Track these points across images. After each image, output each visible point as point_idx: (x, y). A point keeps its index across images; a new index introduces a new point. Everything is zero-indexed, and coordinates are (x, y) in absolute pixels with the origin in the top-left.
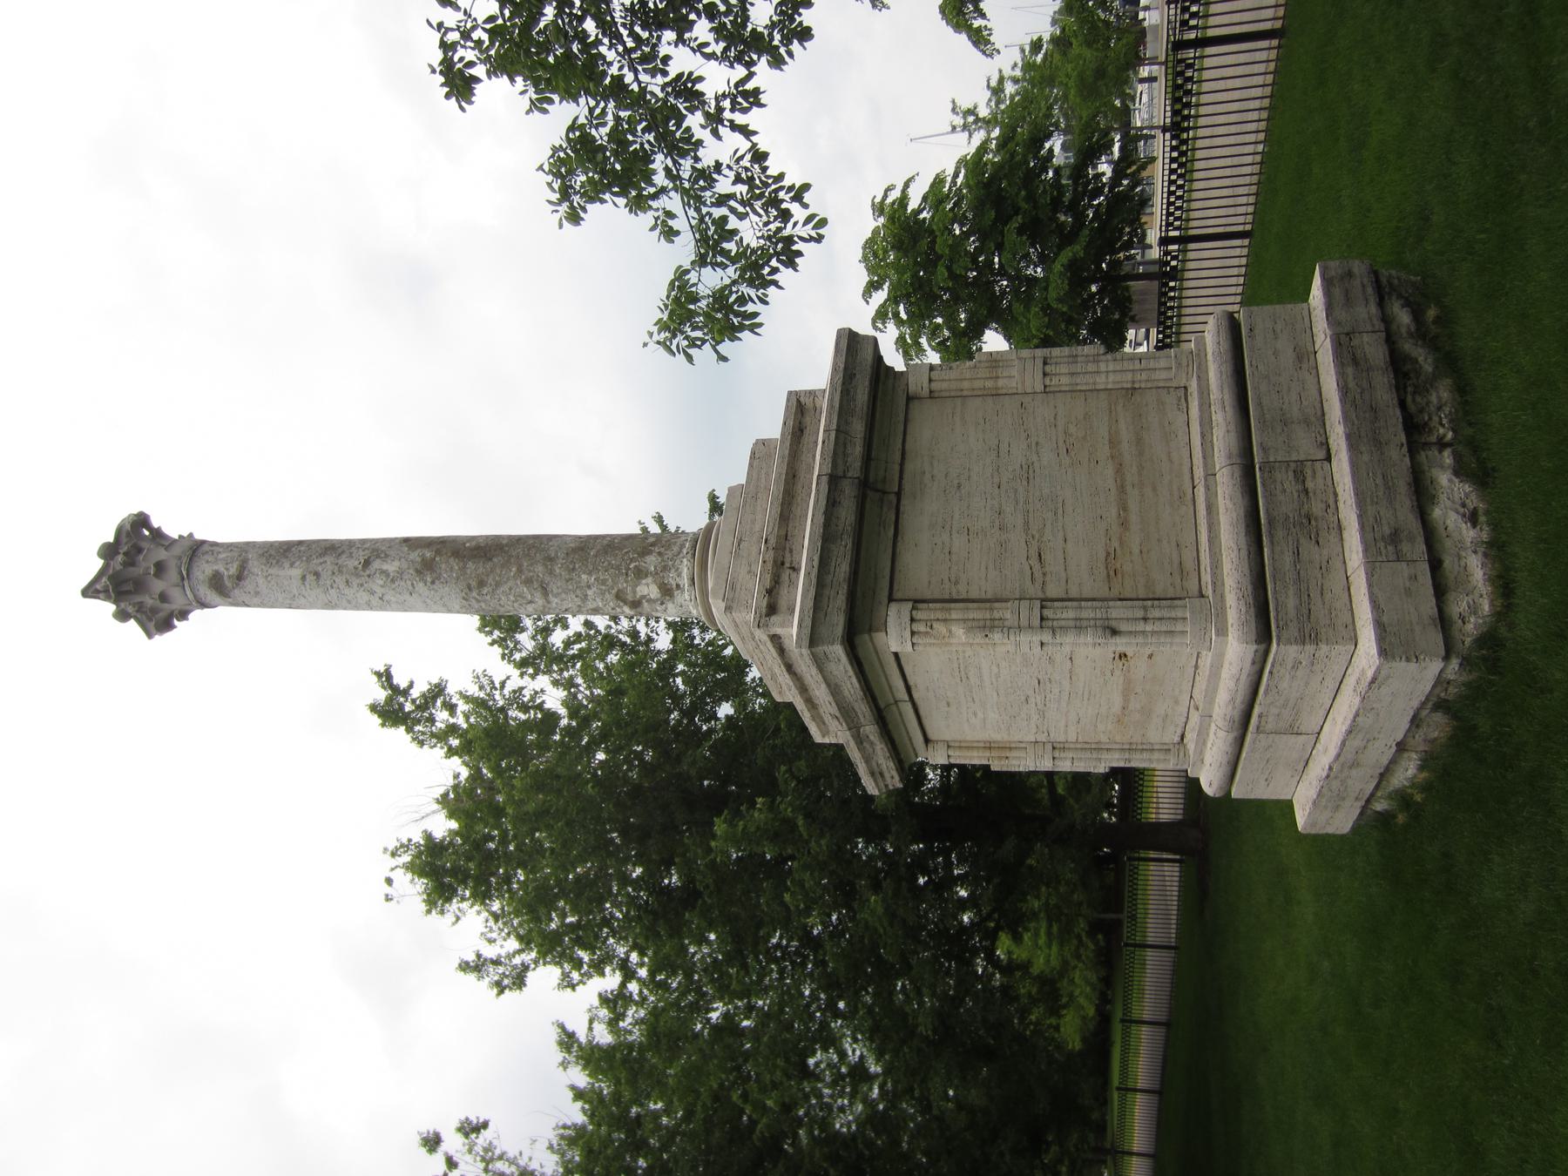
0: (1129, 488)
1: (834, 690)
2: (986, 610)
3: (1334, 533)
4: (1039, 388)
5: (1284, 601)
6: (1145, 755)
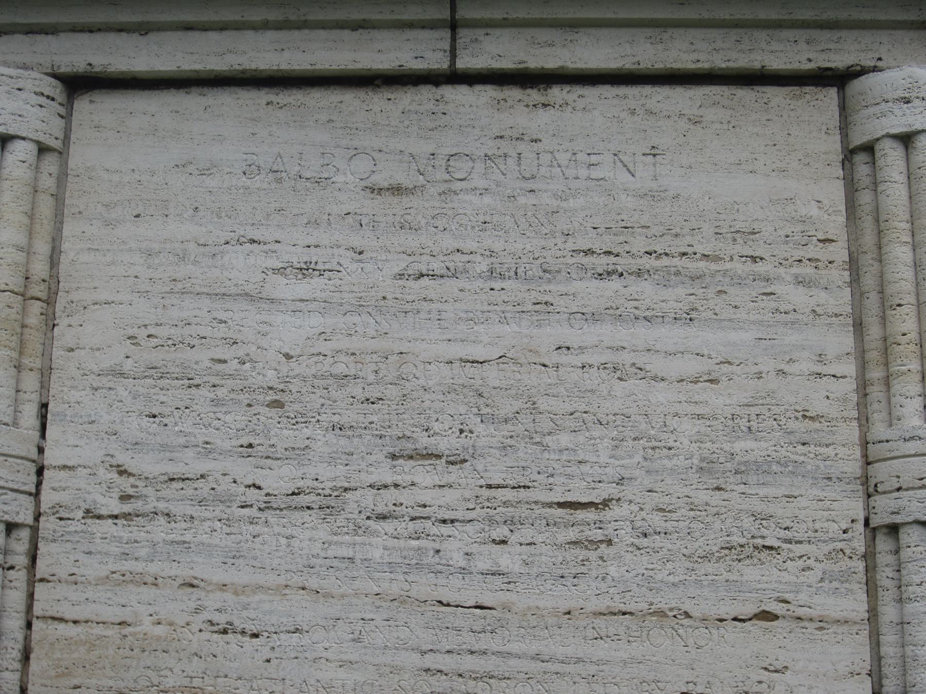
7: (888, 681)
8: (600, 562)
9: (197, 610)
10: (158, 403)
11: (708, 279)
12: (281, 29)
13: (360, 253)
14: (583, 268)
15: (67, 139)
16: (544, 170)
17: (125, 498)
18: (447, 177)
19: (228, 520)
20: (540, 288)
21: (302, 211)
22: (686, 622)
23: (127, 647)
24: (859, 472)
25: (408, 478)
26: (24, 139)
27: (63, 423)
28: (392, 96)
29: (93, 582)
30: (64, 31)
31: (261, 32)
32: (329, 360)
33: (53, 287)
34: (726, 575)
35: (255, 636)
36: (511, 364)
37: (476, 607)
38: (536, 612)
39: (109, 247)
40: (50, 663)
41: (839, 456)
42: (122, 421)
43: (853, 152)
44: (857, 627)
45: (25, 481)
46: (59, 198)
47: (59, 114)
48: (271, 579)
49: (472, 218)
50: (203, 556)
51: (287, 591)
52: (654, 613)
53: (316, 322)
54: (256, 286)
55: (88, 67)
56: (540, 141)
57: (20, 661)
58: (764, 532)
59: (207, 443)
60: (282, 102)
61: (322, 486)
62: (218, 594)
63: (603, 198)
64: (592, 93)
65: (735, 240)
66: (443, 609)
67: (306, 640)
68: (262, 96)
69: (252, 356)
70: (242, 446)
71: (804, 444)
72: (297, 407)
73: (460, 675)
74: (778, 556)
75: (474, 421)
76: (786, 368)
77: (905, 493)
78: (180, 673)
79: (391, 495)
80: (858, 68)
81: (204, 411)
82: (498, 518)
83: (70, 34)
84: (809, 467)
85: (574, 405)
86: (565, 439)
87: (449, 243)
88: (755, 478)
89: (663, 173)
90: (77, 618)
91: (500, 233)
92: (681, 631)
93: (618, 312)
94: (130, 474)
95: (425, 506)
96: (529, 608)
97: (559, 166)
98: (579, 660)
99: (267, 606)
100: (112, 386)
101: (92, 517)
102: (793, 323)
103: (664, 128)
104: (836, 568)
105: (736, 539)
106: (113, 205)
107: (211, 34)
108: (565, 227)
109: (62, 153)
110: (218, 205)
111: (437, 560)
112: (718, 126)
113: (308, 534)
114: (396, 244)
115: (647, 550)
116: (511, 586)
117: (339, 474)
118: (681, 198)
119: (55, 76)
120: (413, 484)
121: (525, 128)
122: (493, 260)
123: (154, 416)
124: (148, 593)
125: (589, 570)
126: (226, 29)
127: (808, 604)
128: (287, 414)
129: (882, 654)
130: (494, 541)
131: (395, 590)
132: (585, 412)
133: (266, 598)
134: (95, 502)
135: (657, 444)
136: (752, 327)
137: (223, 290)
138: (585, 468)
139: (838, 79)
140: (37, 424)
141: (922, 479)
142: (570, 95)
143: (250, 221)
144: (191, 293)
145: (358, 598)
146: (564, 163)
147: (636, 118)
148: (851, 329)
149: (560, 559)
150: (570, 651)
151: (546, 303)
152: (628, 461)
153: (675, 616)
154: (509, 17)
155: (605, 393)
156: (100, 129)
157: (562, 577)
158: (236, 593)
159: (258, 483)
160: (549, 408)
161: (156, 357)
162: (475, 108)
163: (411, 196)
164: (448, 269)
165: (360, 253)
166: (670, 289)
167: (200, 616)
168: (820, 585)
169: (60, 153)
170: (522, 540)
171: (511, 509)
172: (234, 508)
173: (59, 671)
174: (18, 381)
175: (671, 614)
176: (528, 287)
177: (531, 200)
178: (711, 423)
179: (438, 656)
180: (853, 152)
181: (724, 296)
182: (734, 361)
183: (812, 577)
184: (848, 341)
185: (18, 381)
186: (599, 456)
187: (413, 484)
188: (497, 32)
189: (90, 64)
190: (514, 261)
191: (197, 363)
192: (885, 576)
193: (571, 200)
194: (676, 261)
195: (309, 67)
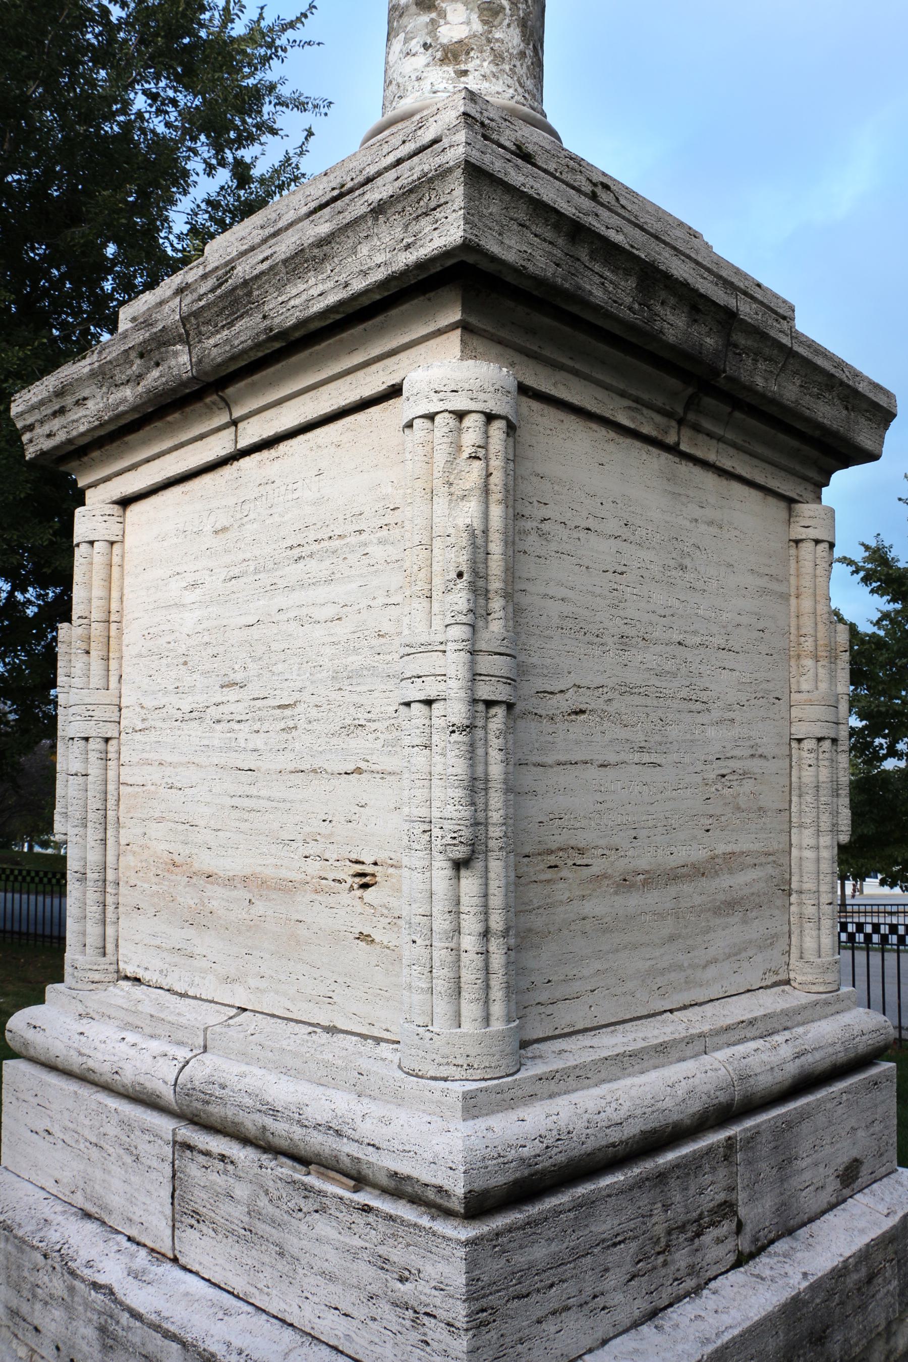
0: (673, 890)
1: (300, 263)
2: (502, 583)
3: (642, 1305)
4: (799, 730)
5: (542, 1235)
6: (93, 910)
68: (265, 454)
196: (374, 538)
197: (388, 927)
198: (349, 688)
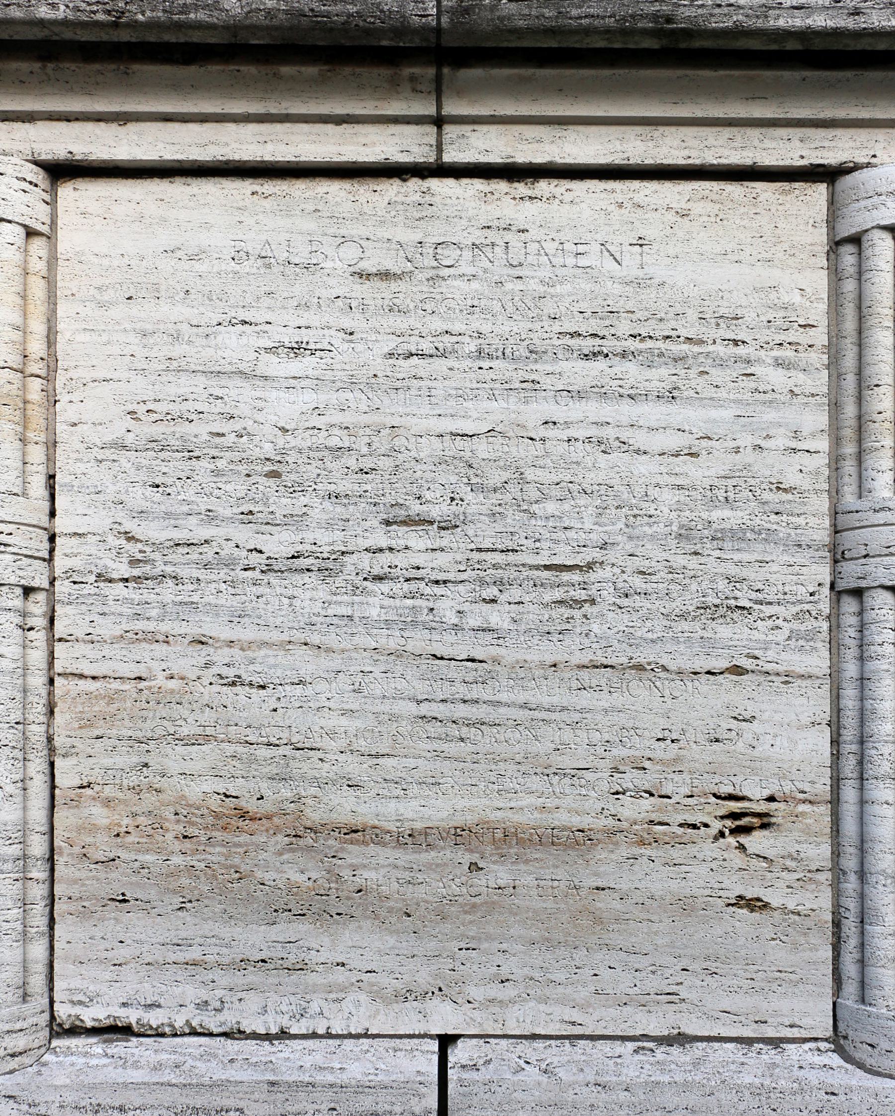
7: (846, 731)
8: (584, 620)
9: (207, 665)
10: (160, 474)
11: (690, 361)
12: (263, 122)
13: (351, 334)
14: (569, 349)
15: (53, 224)
16: (530, 258)
17: (134, 562)
18: (435, 264)
19: (233, 582)
20: (527, 368)
21: (292, 295)
22: (663, 675)
23: (144, 700)
24: (827, 540)
25: (402, 543)
26: (10, 222)
27: (71, 493)
28: (378, 188)
29: (109, 641)
30: (41, 120)
31: (242, 124)
32: (323, 433)
33: (52, 365)
34: (701, 633)
35: (263, 687)
36: (499, 437)
37: (468, 660)
38: (523, 665)
39: (104, 328)
40: (73, 716)
41: (809, 525)
42: (127, 491)
43: (838, 243)
44: (820, 681)
45: (38, 548)
46: (50, 281)
47: (44, 200)
48: (275, 636)
49: (460, 302)
50: (211, 615)
51: (290, 647)
52: (633, 667)
53: (309, 398)
54: (250, 364)
55: (69, 155)
56: (527, 231)
57: (45, 714)
58: (738, 594)
59: (209, 511)
60: (267, 193)
61: (320, 550)
62: (226, 650)
63: (590, 285)
64: (579, 187)
65: (718, 325)
66: (437, 662)
67: (309, 691)
69: (249, 429)
70: (242, 513)
71: (777, 513)
72: (293, 477)
73: (454, 722)
74: (750, 616)
75: (464, 491)
76: (763, 444)
77: (871, 560)
78: (194, 722)
79: (386, 558)
80: (851, 165)
81: (205, 481)
82: (488, 579)
83: (48, 123)
84: (781, 535)
85: (560, 476)
86: (551, 507)
87: (438, 324)
88: (730, 544)
89: (649, 262)
90: (95, 674)
91: (487, 317)
92: (658, 684)
93: (603, 390)
94: (138, 540)
95: (418, 568)
96: (517, 662)
97: (547, 255)
98: (564, 709)
99: (272, 660)
100: (116, 459)
101: (104, 581)
102: (771, 402)
103: (651, 221)
104: (803, 628)
105: (711, 600)
106: (104, 288)
107: (191, 126)
108: (552, 311)
109: (51, 238)
110: (209, 289)
111: (431, 617)
112: (706, 219)
113: (308, 594)
114: (385, 326)
115: (628, 609)
116: (501, 641)
117: (336, 539)
118: (667, 285)
119: (36, 163)
120: (407, 548)
121: (512, 219)
122: (481, 341)
123: (158, 486)
124: (160, 649)
125: (573, 627)
126: (207, 121)
127: (776, 660)
128: (284, 484)
129: (842, 706)
130: (484, 599)
131: (392, 644)
132: (571, 482)
133: (270, 652)
134: (106, 567)
135: (638, 512)
136: (732, 405)
137: (218, 369)
138: (571, 534)
139: (827, 175)
140: (46, 494)
141: (889, 547)
142: (558, 189)
143: (241, 304)
144: (187, 371)
145: (357, 652)
146: (551, 252)
147: (623, 211)
148: (827, 408)
149: (547, 617)
150: (555, 700)
151: (533, 381)
152: (611, 528)
153: (652, 670)
154: (496, 114)
155: (590, 465)
156: (87, 216)
157: (548, 633)
158: (242, 649)
159: (258, 547)
160: (536, 479)
161: (157, 431)
162: (462, 200)
163: (399, 280)
164: (437, 349)
165: (351, 334)
166: (654, 370)
167: (210, 670)
168: (788, 642)
169: (49, 238)
170: (511, 600)
171: (500, 571)
172: (237, 571)
173: (82, 722)
174: (24, 454)
175: (649, 668)
176: (515, 367)
177: (519, 285)
178: (690, 494)
179: (433, 704)
180: (838, 243)
181: (706, 376)
182: (714, 436)
183: (781, 636)
184: (823, 420)
185: (24, 454)
186: (583, 523)
187: (407, 548)
188: (484, 128)
189: (71, 153)
190: (502, 342)
191: (196, 436)
192: (850, 634)
193: (558, 287)
194: (660, 344)
195: (294, 159)
196: (768, 356)
197: (796, 885)
198: (717, 553)
